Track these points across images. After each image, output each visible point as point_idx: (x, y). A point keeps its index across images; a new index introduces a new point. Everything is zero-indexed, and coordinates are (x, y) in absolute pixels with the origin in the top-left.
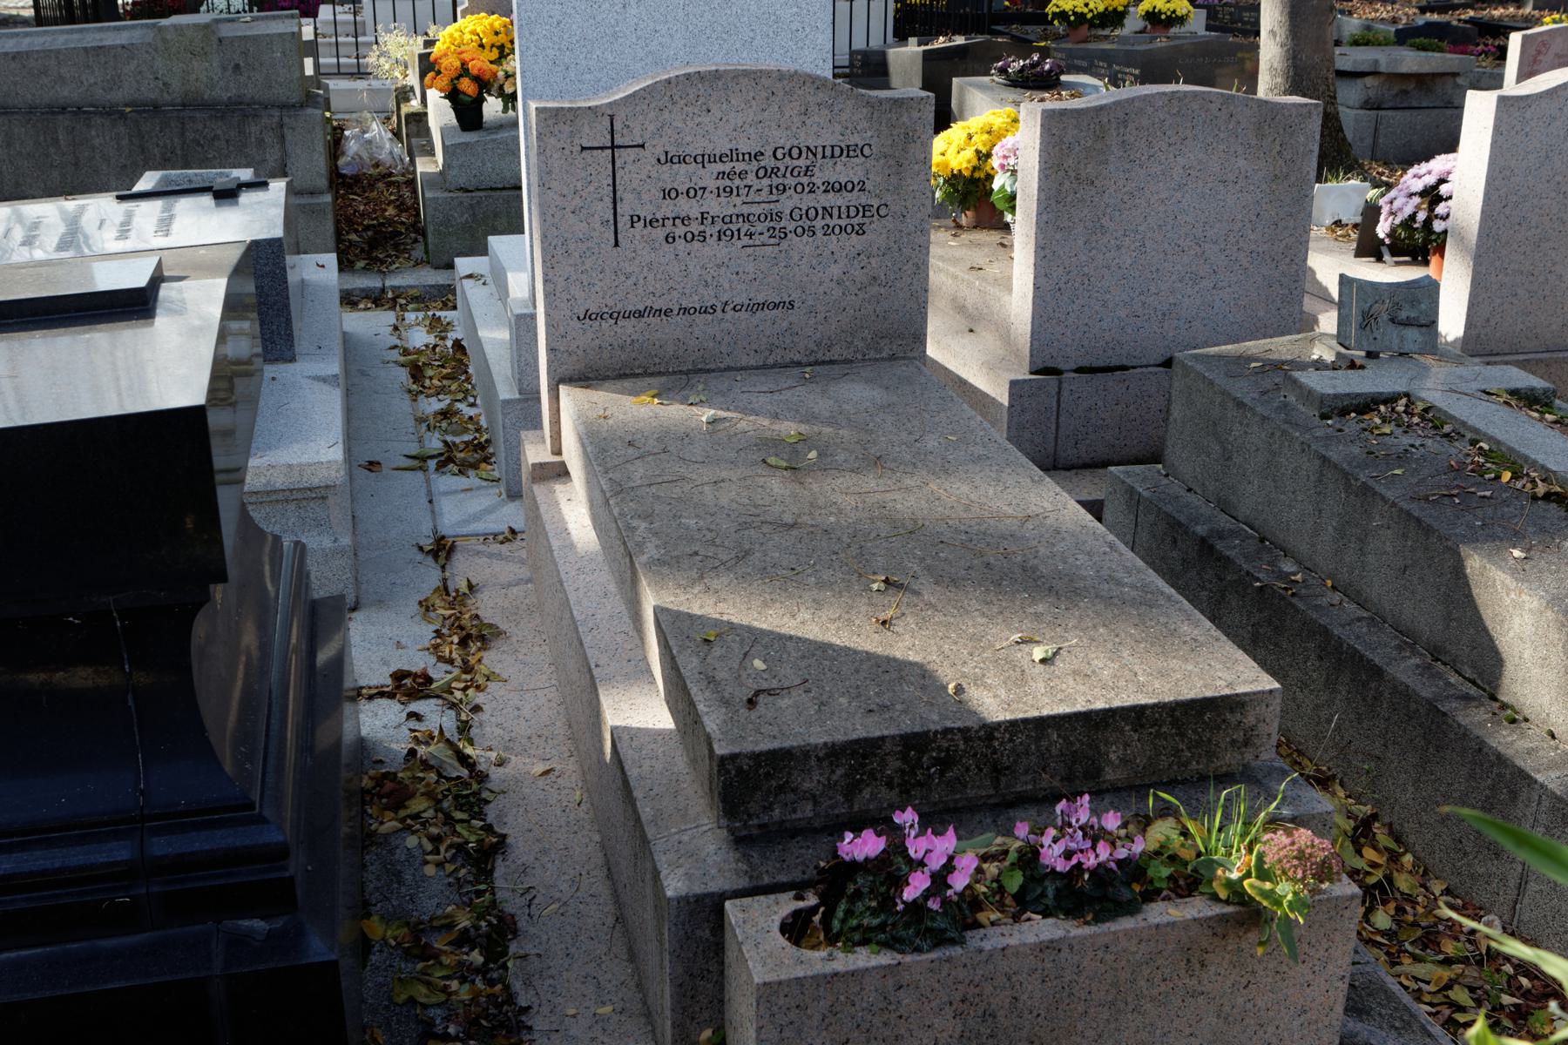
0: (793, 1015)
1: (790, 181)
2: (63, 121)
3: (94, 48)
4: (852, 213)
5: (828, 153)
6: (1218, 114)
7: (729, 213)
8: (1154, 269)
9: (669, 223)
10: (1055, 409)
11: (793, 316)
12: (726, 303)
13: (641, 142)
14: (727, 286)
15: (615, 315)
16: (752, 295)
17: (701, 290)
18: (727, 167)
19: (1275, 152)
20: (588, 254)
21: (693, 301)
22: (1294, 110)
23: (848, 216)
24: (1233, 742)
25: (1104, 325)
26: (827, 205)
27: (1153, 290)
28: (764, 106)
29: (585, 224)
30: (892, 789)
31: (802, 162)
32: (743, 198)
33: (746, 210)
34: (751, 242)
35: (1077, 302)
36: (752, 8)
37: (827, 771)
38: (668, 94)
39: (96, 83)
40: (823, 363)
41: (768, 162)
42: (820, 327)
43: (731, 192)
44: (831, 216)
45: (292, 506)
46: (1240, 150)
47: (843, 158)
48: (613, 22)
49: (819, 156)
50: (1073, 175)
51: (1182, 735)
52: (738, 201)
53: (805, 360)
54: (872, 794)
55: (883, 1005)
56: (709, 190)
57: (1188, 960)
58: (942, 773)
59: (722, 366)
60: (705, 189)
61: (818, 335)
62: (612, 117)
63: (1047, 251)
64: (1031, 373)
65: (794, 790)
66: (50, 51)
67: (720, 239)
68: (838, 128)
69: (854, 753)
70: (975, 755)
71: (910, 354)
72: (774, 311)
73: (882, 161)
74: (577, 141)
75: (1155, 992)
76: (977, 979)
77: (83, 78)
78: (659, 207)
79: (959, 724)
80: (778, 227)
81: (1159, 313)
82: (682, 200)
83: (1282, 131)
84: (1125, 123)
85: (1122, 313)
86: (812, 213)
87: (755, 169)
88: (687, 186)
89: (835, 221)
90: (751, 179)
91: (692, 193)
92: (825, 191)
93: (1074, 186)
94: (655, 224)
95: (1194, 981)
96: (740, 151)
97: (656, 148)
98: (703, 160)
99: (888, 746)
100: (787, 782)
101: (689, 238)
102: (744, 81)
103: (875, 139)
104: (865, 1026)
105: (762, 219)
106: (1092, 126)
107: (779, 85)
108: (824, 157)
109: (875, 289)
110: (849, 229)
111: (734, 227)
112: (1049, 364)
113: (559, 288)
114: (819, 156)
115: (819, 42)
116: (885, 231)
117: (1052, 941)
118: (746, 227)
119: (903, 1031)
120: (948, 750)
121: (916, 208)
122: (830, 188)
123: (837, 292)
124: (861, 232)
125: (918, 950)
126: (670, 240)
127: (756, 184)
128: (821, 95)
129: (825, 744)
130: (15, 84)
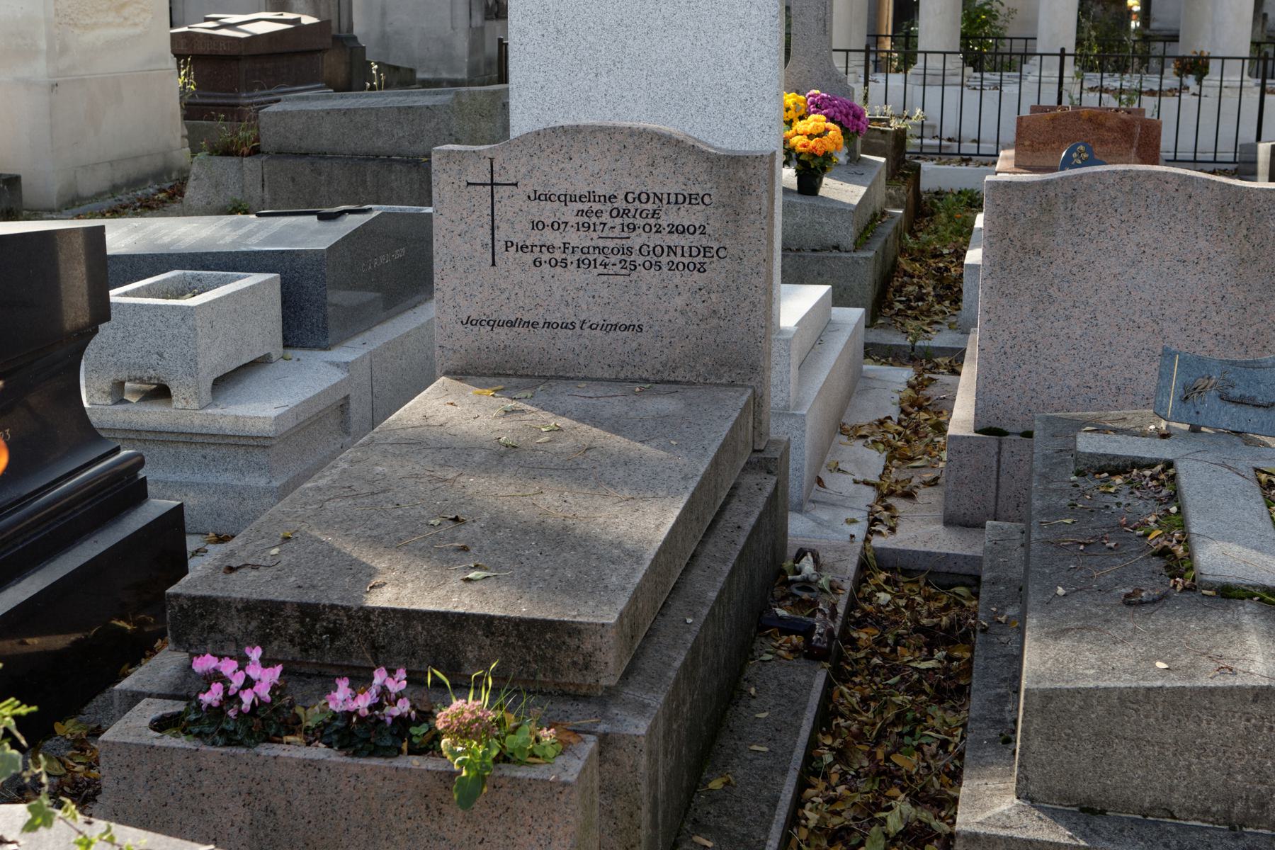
0: (125, 772)
1: (639, 222)
2: (372, 166)
3: (405, 108)
4: (695, 252)
5: (673, 199)
6: (1176, 195)
7: (587, 245)
8: (1106, 342)
9: (537, 249)
10: (995, 468)
11: (643, 338)
12: (584, 322)
13: (514, 181)
14: (584, 307)
15: (492, 323)
16: (606, 317)
17: (563, 308)
18: (585, 206)
19: (1240, 235)
20: (471, 270)
21: (555, 318)
22: (1261, 195)
23: (691, 255)
24: (574, 663)
25: (1054, 392)
26: (672, 244)
27: (1106, 363)
28: (618, 157)
29: (468, 245)
30: (294, 646)
31: (650, 206)
32: (599, 233)
33: (601, 243)
34: (605, 271)
35: (1024, 367)
36: (706, 79)
37: (245, 621)
38: (538, 143)
39: (404, 137)
40: (669, 382)
41: (621, 204)
42: (666, 350)
43: (589, 227)
44: (675, 254)
45: (241, 451)
46: (1201, 231)
47: (686, 205)
48: (587, 88)
49: (665, 202)
50: (1019, 244)
51: (529, 649)
52: (595, 235)
53: (652, 378)
54: (279, 647)
55: (190, 781)
56: (570, 224)
57: (427, 807)
58: (332, 641)
59: (580, 375)
60: (567, 223)
61: (664, 357)
62: (492, 160)
63: (992, 315)
64: (976, 432)
65: (221, 632)
66: (372, 109)
67: (579, 267)
68: (682, 179)
69: (263, 611)
70: (357, 631)
71: (747, 383)
72: (626, 332)
73: (721, 210)
74: (464, 178)
75: (403, 827)
76: (258, 778)
77: (395, 131)
78: (528, 236)
79: (345, 603)
80: (629, 260)
81: (1113, 387)
82: (547, 231)
83: (1248, 216)
84: (1073, 198)
85: (1073, 383)
86: (658, 250)
87: (609, 209)
88: (552, 220)
89: (678, 259)
90: (605, 217)
91: (557, 226)
92: (669, 232)
93: (1020, 255)
94: (525, 250)
95: (434, 826)
96: (597, 193)
97: (527, 187)
98: (566, 199)
99: (288, 611)
100: (215, 624)
101: (554, 263)
102: (600, 135)
103: (714, 190)
104: (178, 795)
105: (615, 252)
106: (1038, 199)
107: (631, 140)
108: (669, 203)
109: (714, 322)
110: (691, 266)
111: (591, 258)
112: (995, 425)
113: (447, 297)
114: (665, 202)
115: (766, 110)
116: (724, 270)
117: (312, 760)
118: (600, 258)
119: (206, 807)
120: (335, 623)
121: (752, 253)
122: (674, 229)
123: (681, 321)
124: (702, 269)
125: (214, 744)
126: (538, 264)
127: (610, 222)
128: (666, 150)
129: (242, 599)
130: (343, 134)
